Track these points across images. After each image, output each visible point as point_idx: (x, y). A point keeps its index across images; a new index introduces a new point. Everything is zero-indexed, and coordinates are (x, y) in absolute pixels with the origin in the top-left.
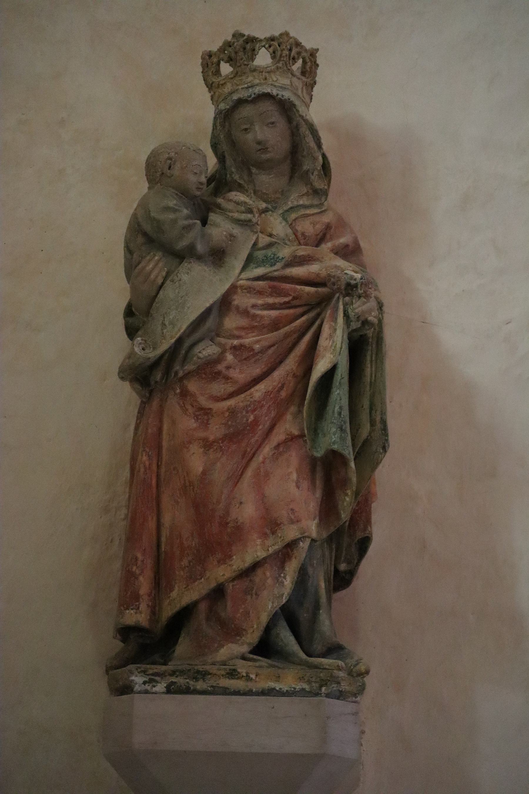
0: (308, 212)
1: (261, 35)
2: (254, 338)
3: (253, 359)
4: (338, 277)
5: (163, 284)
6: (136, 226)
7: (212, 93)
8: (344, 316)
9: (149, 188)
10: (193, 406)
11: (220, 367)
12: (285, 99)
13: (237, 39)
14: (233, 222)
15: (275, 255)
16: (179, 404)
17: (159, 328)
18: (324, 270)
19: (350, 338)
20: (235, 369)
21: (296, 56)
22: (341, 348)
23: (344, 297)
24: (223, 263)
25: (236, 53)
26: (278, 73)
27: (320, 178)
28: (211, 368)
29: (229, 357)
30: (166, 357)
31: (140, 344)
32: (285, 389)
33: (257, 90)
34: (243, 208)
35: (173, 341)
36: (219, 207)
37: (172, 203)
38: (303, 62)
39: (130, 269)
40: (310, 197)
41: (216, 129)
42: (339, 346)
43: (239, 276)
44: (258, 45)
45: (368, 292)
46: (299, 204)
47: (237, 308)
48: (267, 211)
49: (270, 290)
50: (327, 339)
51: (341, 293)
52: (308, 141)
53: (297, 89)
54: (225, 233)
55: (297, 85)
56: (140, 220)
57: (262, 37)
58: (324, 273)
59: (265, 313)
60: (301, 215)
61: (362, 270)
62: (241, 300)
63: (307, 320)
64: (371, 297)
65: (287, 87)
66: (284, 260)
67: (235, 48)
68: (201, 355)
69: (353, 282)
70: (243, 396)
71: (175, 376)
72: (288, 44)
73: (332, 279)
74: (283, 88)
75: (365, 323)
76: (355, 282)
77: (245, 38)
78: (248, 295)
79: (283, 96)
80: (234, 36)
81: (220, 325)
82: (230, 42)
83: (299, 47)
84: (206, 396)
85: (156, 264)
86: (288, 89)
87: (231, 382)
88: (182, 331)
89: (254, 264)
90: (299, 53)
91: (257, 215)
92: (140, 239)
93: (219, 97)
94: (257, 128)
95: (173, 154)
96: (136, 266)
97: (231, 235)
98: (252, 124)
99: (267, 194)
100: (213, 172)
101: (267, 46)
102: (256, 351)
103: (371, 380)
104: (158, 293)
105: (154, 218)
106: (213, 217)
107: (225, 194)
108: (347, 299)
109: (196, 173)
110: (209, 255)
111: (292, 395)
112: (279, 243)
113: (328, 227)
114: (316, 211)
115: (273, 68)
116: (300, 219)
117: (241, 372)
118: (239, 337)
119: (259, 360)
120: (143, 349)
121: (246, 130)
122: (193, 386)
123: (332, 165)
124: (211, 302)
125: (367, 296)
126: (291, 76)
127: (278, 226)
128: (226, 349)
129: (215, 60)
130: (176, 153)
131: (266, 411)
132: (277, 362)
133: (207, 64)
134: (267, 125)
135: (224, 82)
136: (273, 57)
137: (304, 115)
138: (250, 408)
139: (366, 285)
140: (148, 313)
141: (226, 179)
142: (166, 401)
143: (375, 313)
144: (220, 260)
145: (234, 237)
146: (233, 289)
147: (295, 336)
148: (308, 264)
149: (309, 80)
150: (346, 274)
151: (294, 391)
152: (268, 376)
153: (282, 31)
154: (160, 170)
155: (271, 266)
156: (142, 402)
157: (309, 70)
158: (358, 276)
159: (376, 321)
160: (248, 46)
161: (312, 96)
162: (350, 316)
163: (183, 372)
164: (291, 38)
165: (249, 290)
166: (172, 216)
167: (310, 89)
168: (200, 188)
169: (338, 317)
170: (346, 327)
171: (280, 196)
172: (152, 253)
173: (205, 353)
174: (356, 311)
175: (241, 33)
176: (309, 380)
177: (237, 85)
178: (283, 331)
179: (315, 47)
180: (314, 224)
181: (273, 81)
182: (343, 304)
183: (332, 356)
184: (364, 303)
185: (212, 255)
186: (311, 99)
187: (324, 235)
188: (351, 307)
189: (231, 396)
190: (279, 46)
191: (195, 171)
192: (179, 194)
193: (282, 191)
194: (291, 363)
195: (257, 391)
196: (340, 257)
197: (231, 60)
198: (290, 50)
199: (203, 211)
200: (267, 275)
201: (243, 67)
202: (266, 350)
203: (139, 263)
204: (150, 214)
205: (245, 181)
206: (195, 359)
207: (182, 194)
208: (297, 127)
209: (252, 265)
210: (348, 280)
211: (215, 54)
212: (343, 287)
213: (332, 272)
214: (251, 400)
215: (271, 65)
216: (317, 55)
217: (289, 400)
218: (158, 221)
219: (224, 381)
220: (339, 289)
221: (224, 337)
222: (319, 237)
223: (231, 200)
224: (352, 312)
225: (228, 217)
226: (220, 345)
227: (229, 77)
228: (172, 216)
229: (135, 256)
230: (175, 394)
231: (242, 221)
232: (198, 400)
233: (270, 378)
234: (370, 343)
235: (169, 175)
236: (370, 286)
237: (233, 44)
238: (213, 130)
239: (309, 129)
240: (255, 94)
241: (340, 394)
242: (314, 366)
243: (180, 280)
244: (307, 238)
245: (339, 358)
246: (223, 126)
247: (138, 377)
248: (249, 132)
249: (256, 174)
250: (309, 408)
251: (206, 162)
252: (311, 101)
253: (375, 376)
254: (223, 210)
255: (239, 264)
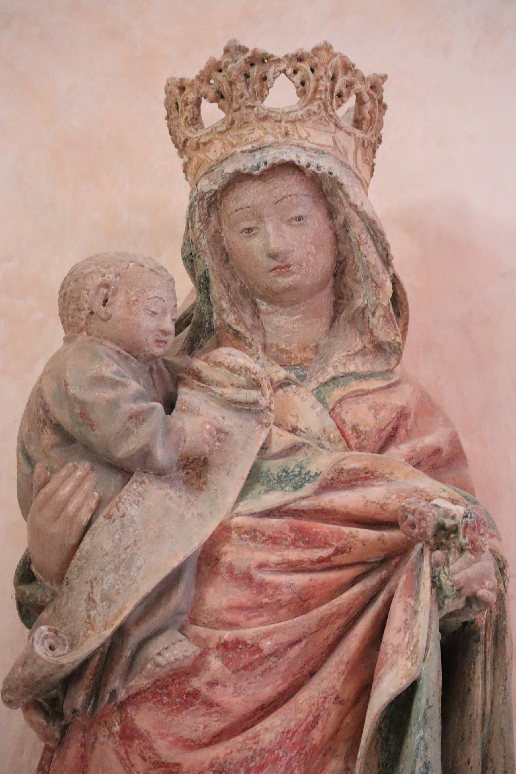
0: (365, 385)
1: (279, 48)
2: (263, 628)
3: (261, 669)
4: (421, 514)
5: (90, 523)
6: (41, 412)
7: (186, 159)
8: (432, 588)
9: (67, 340)
10: (144, 759)
11: (197, 683)
12: (323, 174)
13: (232, 57)
14: (223, 406)
15: (302, 468)
16: (117, 753)
17: (83, 605)
18: (394, 497)
19: (442, 630)
20: (225, 686)
21: (345, 91)
22: (427, 650)
23: (432, 550)
24: (205, 483)
25: (231, 84)
26: (310, 123)
27: (387, 321)
28: (180, 684)
29: (215, 663)
30: (95, 662)
31: (46, 637)
32: (320, 725)
33: (273, 156)
34: (242, 380)
35: (109, 632)
36: (197, 376)
37: (109, 369)
38: (357, 100)
39: (28, 494)
40: (368, 357)
41: (193, 227)
42: (422, 644)
43: (233, 509)
44: (272, 70)
45: (478, 543)
46: (347, 371)
47: (231, 569)
48: (289, 384)
49: (292, 535)
50: (399, 631)
51: (427, 543)
52: (365, 253)
53: (346, 154)
54: (208, 427)
55: (346, 146)
56: (49, 400)
57: (280, 54)
58: (394, 504)
59: (283, 579)
60: (352, 392)
61: (465, 497)
62: (237, 554)
63: (363, 593)
64: (484, 552)
65: (327, 150)
66: (320, 478)
67: (230, 74)
68: (160, 660)
69: (449, 523)
70: (240, 738)
71: (109, 702)
72: (329, 66)
73: (410, 517)
74: (320, 152)
75: (472, 600)
76: (453, 522)
77: (249, 54)
78: (252, 545)
79: (318, 167)
80: (227, 50)
81: (198, 600)
82: (220, 63)
83: (350, 74)
84: (170, 739)
85: (78, 486)
86: (329, 153)
87: (217, 712)
88: (126, 613)
89: (263, 485)
90: (349, 85)
91: (268, 393)
92: (48, 437)
93: (199, 165)
94: (270, 227)
95: (112, 276)
96: (40, 488)
97: (219, 431)
98: (260, 218)
99: (289, 352)
100: (186, 307)
101: (290, 71)
102: (266, 652)
103: (484, 709)
104: (80, 540)
105: (75, 398)
106: (186, 395)
107: (210, 350)
108: (438, 554)
109: (154, 313)
110: (179, 468)
111: (334, 736)
112: (309, 446)
113: (403, 414)
114: (379, 383)
115: (300, 113)
116: (350, 400)
117: (237, 692)
118: (232, 625)
119: (270, 669)
120: (51, 648)
121: (249, 230)
122: (144, 719)
123: (410, 296)
124: (181, 558)
125: (475, 549)
126: (333, 127)
127: (307, 412)
128: (209, 649)
129: (191, 97)
130: (118, 275)
131: (283, 769)
132: (305, 673)
133: (177, 103)
134: (289, 222)
135: (207, 139)
136: (302, 94)
137: (358, 203)
138: (252, 764)
139: (474, 529)
140: (61, 578)
141: (210, 323)
142: (93, 748)
143: (491, 582)
144: (199, 476)
145: (227, 433)
146: (223, 533)
147: (340, 622)
148: (363, 486)
149: (368, 136)
150: (436, 506)
151: (337, 731)
152: (286, 701)
153: (318, 41)
154: (86, 306)
155: (295, 489)
156: (47, 748)
157: (368, 116)
158: (459, 510)
159: (492, 597)
160: (254, 72)
161: (373, 165)
162: (444, 587)
163: (127, 692)
164: (335, 55)
165: (253, 534)
166: (109, 394)
167: (371, 152)
168: (163, 341)
169: (422, 588)
170: (435, 608)
171: (313, 356)
172: (71, 464)
173: (169, 656)
174: (456, 577)
175: (240, 47)
176: (366, 707)
177: (233, 146)
178: (316, 614)
179: (380, 71)
180: (376, 409)
181: (300, 138)
182: (431, 564)
183: (409, 664)
184: (470, 564)
185: (185, 467)
186: (372, 170)
187: (396, 429)
188: (446, 570)
189: (217, 738)
190: (313, 71)
191: (153, 309)
192: (122, 352)
193: (317, 347)
194: (331, 677)
195: (267, 729)
196: (425, 472)
197: (222, 97)
198: (334, 78)
199: (168, 386)
200: (287, 507)
201: (244, 111)
202: (285, 651)
203: (45, 483)
204: (67, 391)
205: (246, 327)
206: (149, 666)
207: (128, 352)
208: (346, 226)
209: (259, 488)
210: (442, 518)
211: (192, 85)
212: (430, 532)
213: (410, 503)
214: (255, 747)
215: (297, 107)
216: (384, 86)
217: (327, 750)
218: (83, 404)
219: (203, 710)
220: (423, 535)
221: (205, 625)
222: (384, 434)
223: (219, 364)
224: (448, 579)
225: (214, 396)
226: (196, 639)
227: (219, 129)
228: (109, 394)
229: (38, 467)
230: (111, 734)
231: (241, 403)
232: (155, 746)
233: (291, 704)
234: (482, 639)
235: (103, 316)
236: (482, 531)
237: (226, 67)
238: (188, 228)
239: (368, 229)
240: (266, 163)
241: (424, 736)
242: (375, 683)
243: (124, 516)
244: (363, 437)
245: (424, 667)
246: (206, 223)
247: (40, 700)
248: (255, 235)
249: (268, 314)
250: (366, 764)
251: (173, 290)
252: (372, 175)
253: (492, 705)
254: (204, 382)
255: (234, 485)
